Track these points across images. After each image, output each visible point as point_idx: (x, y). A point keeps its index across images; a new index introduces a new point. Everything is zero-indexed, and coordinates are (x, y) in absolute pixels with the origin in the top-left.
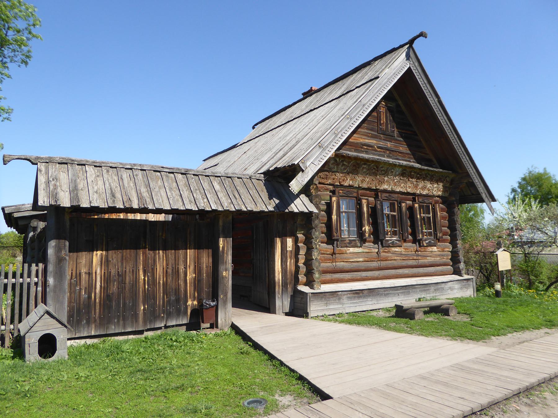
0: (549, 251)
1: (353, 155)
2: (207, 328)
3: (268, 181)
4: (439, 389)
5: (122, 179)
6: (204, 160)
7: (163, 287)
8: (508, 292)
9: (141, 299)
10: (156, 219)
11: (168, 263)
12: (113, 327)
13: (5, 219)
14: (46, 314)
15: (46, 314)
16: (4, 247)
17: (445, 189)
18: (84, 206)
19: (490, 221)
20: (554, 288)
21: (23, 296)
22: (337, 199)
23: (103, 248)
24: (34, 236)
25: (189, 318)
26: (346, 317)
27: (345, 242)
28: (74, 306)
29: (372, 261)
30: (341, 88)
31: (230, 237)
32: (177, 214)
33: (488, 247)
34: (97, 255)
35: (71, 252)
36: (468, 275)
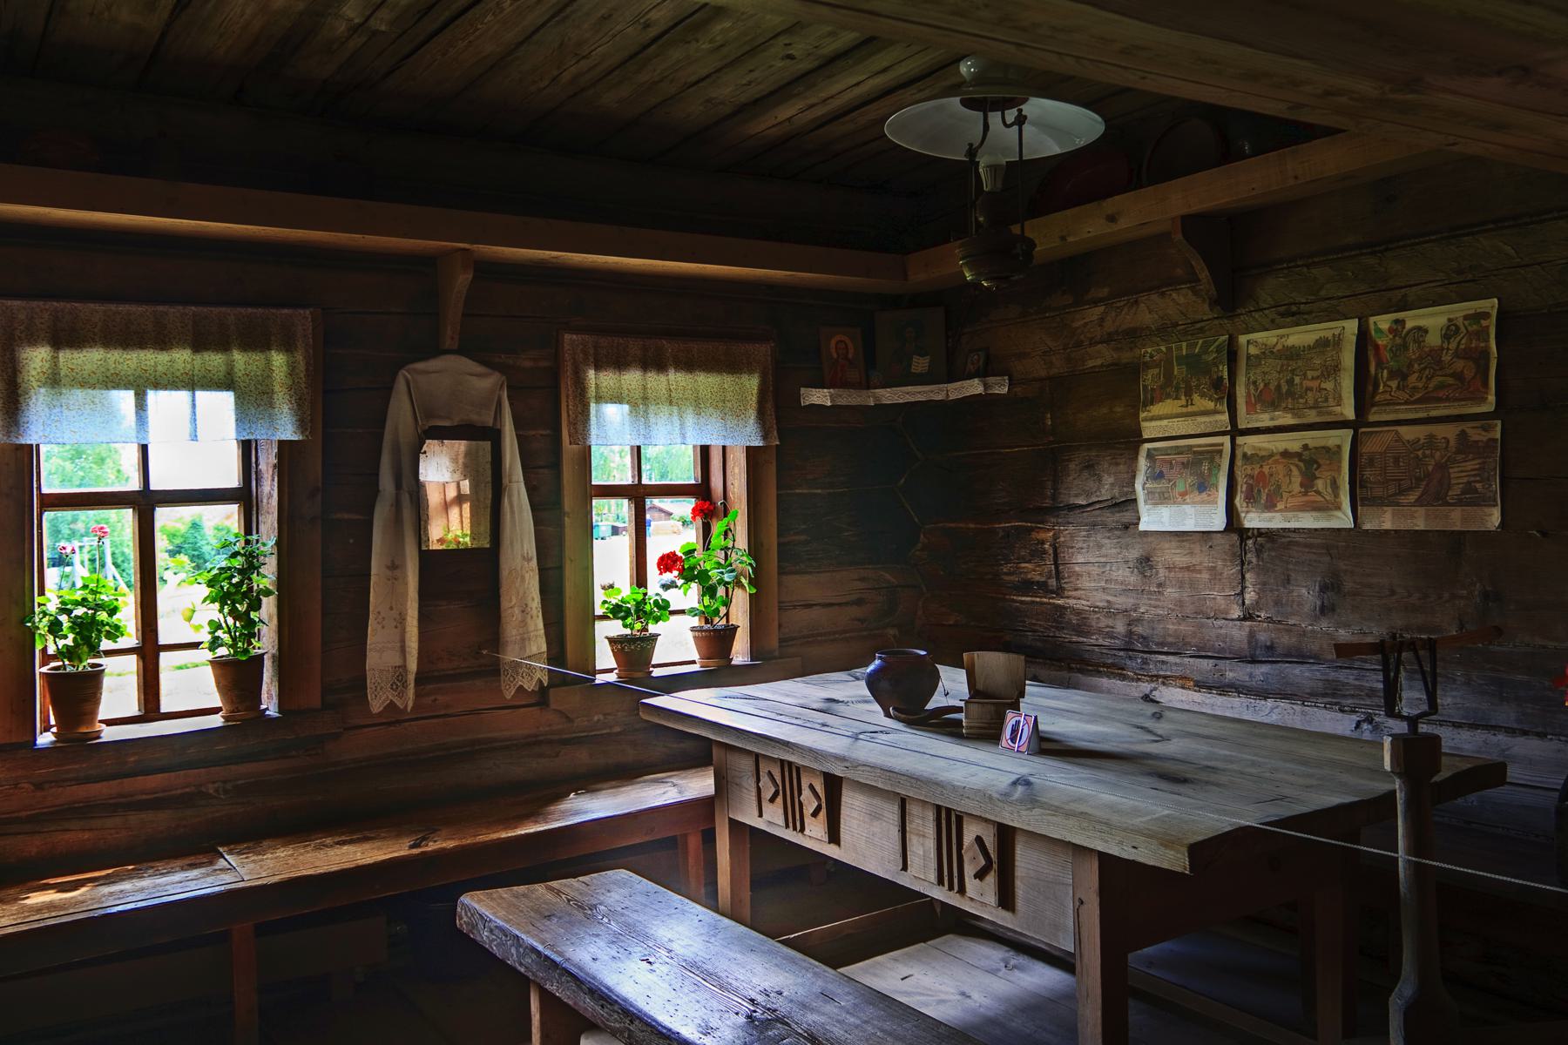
0: (811, 787)
1: (912, 967)
2: (461, 512)
3: (498, 650)
4: (543, 942)
5: (824, 725)
6: (902, 979)
7: (574, 738)
8: (510, 949)
9: (542, 829)
10: (1041, 723)
11: (103, 553)
12: (160, 368)
13: (839, 840)
14: (164, 709)
15: (164, 709)
16: (1127, 611)
17: (33, 341)
18: (434, 548)
19: (122, 412)
20: (910, 823)
21: (1102, 750)
22: (470, 468)
23: (233, 712)
24: (986, 280)
25: (253, 884)
26: (792, 532)
27: (1421, 442)
28: (1251, 408)
29: (1219, 87)
30: (1225, 688)
31: (751, 372)
32: (621, 643)
33: (1000, 557)
34: (1381, 686)
35: (280, 455)
36: (463, 315)
